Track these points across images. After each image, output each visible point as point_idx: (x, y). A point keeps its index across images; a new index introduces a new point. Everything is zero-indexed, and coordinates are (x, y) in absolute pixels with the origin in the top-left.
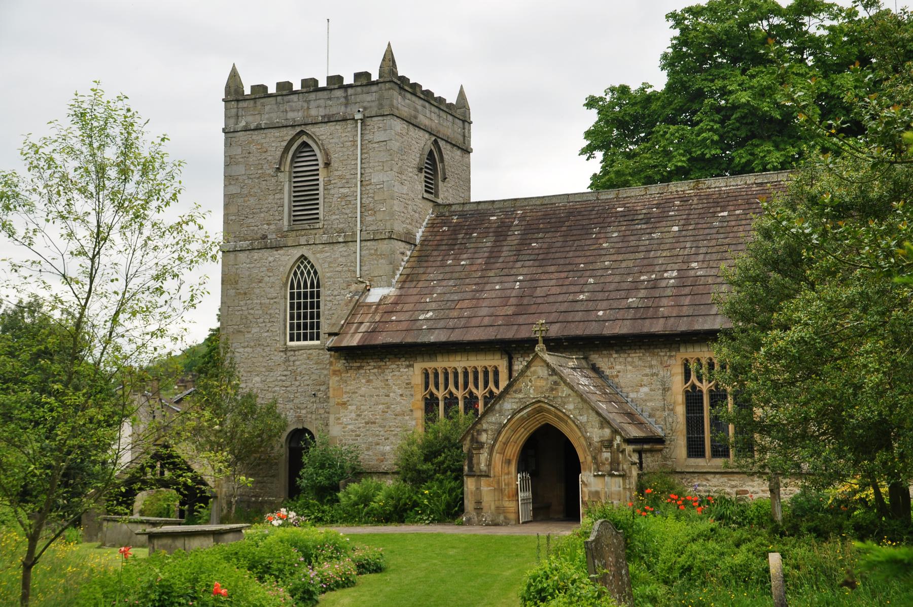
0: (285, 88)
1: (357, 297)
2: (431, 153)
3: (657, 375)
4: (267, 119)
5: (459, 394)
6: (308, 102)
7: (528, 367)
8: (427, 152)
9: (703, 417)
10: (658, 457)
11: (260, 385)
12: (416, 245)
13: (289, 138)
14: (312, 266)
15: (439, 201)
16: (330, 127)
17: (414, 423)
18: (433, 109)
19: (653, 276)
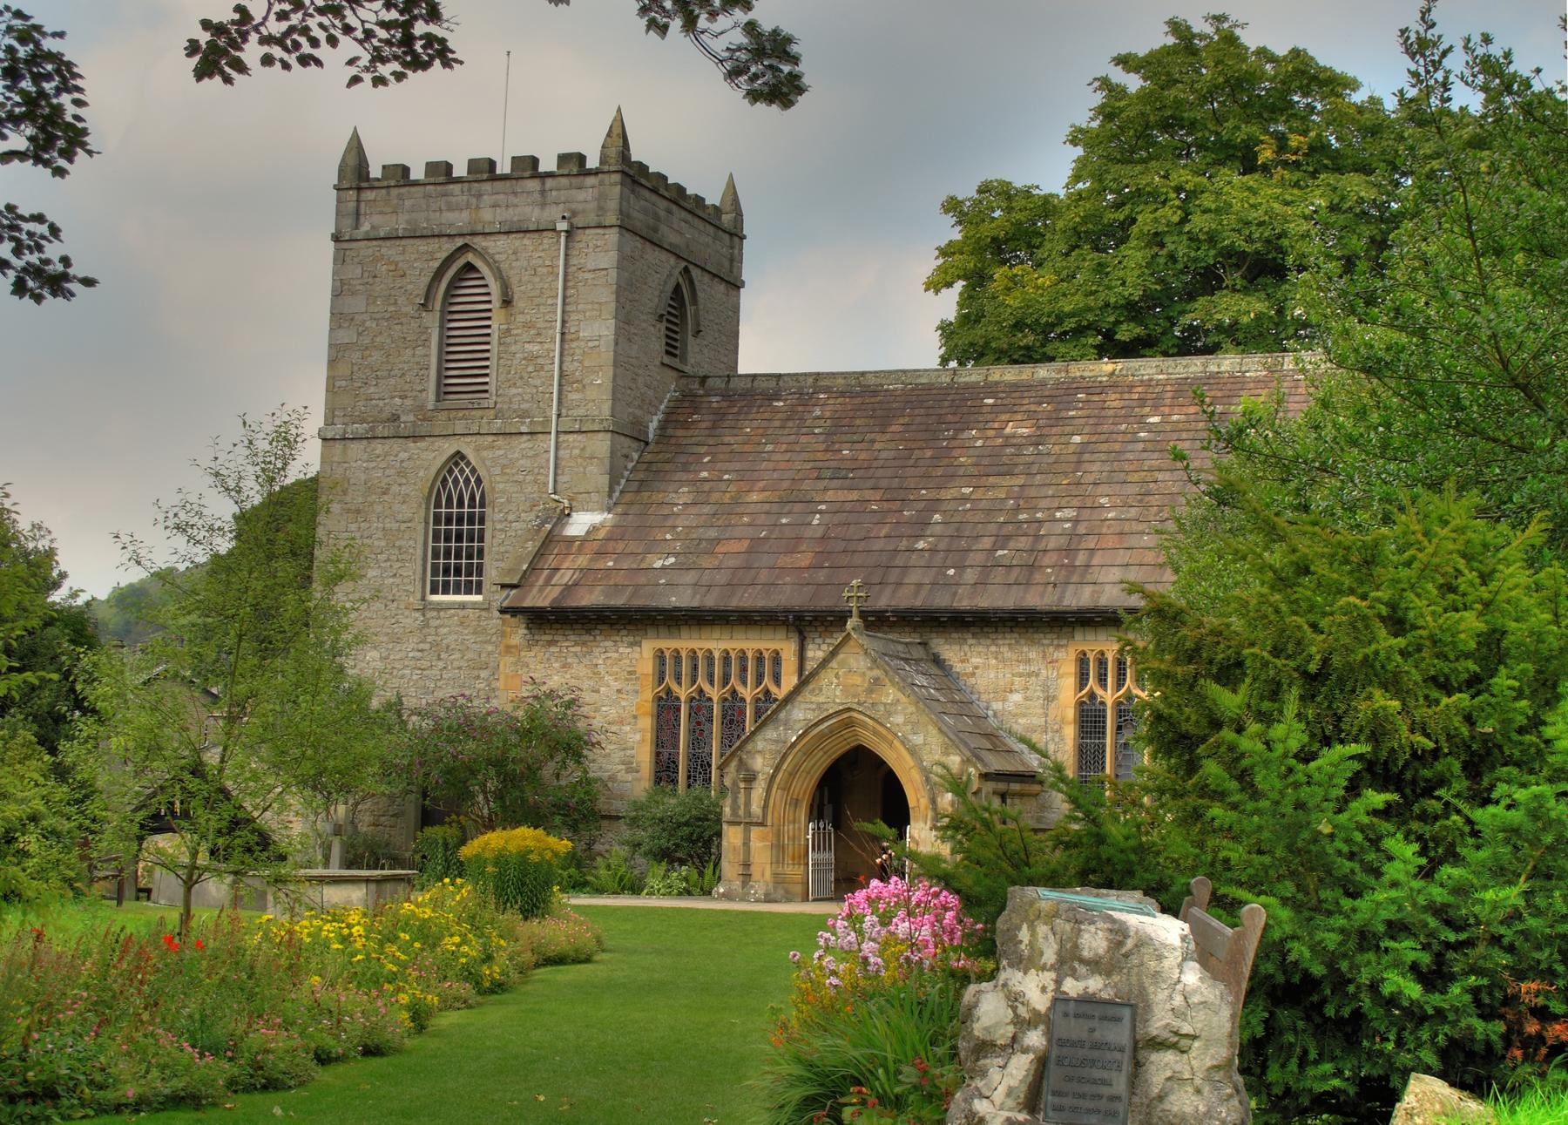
0: (441, 172)
1: (548, 526)
2: (677, 288)
3: (1037, 675)
4: (408, 222)
5: (714, 693)
6: (479, 196)
7: (833, 654)
8: (670, 287)
9: (1104, 745)
10: (1031, 805)
11: (379, 665)
12: (647, 443)
13: (444, 255)
14: (473, 471)
15: (687, 369)
16: (515, 241)
17: (638, 737)
18: (684, 214)
19: (1039, 515)
